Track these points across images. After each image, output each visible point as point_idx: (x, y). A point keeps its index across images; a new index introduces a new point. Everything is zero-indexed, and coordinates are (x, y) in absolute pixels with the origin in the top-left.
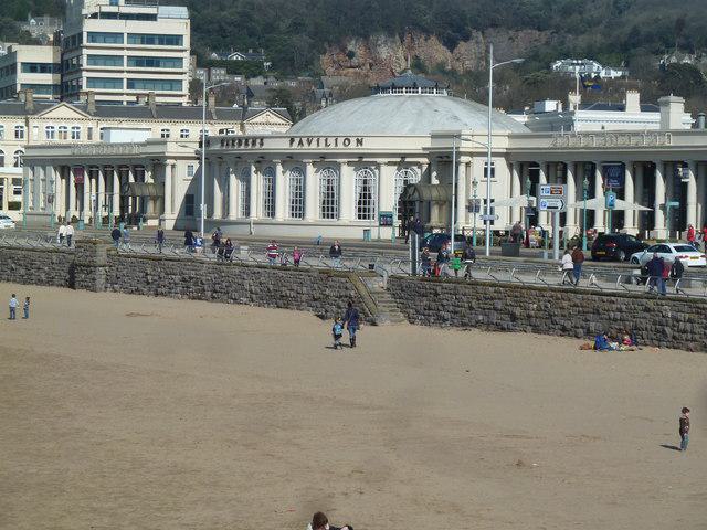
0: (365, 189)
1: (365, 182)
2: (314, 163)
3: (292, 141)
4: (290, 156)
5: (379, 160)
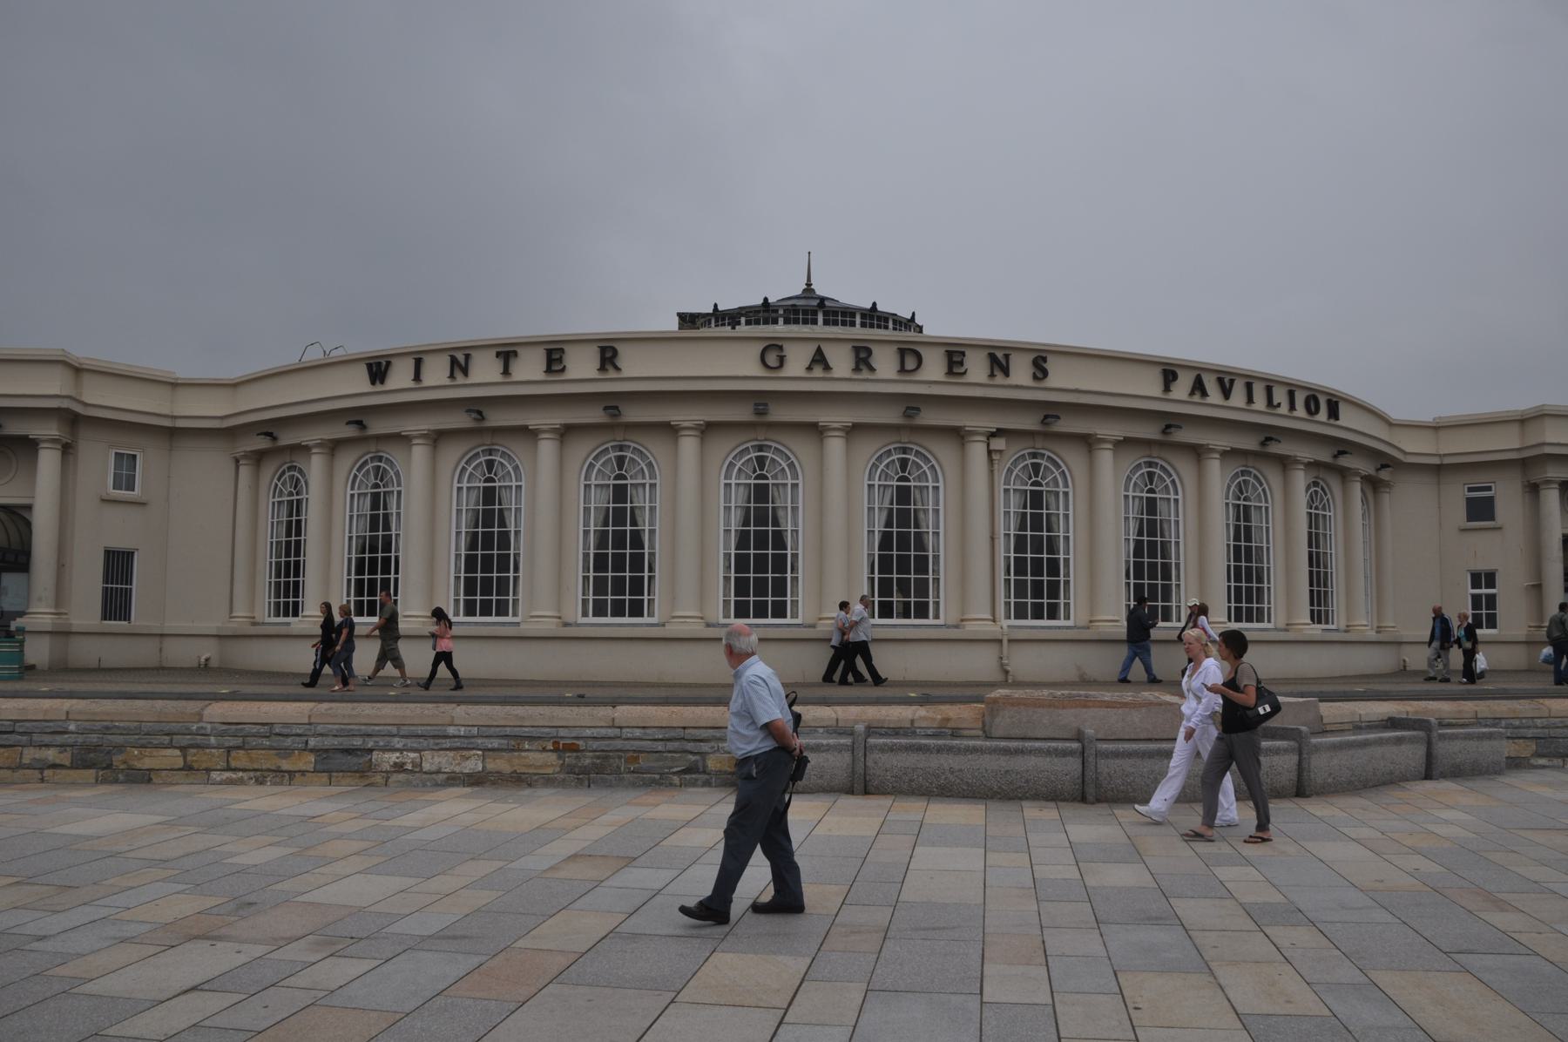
1: (375, 497)
4: (358, 417)
5: (534, 419)
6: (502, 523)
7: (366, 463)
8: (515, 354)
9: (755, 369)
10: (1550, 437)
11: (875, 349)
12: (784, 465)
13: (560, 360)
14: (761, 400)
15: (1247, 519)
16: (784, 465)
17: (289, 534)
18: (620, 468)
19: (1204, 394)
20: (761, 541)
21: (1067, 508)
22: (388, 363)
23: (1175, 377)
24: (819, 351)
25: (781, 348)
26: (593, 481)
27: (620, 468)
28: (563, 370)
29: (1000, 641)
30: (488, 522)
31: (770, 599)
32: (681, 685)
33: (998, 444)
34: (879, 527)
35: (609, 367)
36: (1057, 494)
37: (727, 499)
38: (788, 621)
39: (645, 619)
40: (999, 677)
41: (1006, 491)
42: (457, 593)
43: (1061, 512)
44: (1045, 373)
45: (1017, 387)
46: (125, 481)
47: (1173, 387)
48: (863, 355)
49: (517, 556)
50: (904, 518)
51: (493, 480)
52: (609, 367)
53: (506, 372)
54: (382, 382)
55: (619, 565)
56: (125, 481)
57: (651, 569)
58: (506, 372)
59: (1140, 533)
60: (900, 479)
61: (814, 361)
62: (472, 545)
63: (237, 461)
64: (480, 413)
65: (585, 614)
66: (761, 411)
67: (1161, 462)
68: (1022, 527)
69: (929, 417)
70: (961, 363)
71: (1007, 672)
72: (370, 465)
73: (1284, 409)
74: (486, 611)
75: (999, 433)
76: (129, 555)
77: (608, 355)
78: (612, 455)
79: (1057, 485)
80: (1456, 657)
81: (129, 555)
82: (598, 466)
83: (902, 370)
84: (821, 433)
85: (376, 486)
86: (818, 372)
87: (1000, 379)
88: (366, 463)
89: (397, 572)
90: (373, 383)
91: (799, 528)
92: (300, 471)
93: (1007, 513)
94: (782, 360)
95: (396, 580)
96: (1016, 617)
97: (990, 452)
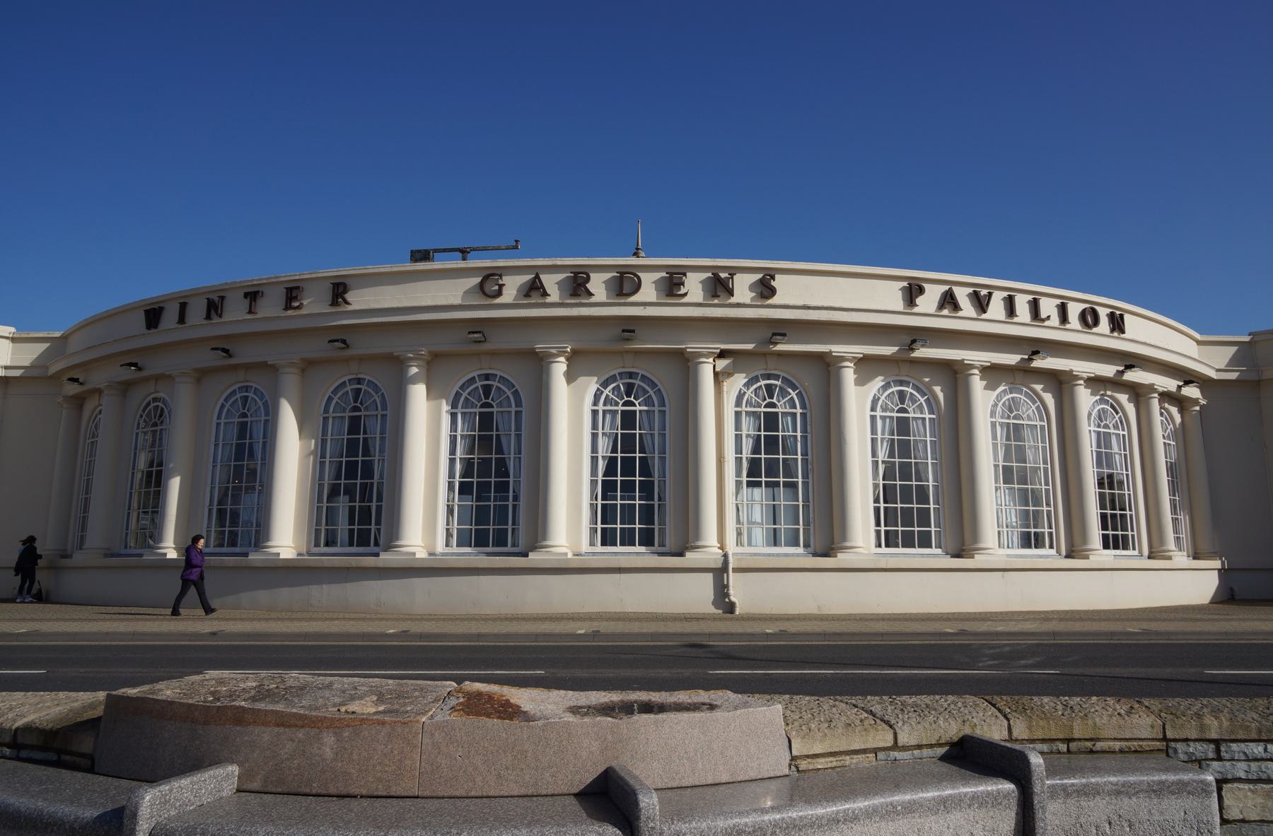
0: (352, 447)
2: (307, 366)
5: (837, 349)
10: (1191, 348)
12: (509, 393)
14: (479, 329)
15: (1019, 437)
16: (509, 393)
18: (487, 397)
19: (956, 307)
20: (905, 475)
23: (921, 291)
27: (487, 397)
31: (619, 526)
32: (486, 619)
34: (746, 453)
38: (509, 549)
41: (738, 414)
44: (773, 292)
45: (739, 305)
47: (919, 300)
49: (380, 485)
57: (380, 499)
60: (482, 406)
64: (344, 342)
65: (592, 544)
67: (912, 381)
72: (238, 396)
73: (1055, 320)
79: (510, 406)
82: (465, 394)
84: (542, 359)
88: (234, 392)
92: (164, 402)
93: (738, 438)
95: (878, 524)
96: (887, 545)
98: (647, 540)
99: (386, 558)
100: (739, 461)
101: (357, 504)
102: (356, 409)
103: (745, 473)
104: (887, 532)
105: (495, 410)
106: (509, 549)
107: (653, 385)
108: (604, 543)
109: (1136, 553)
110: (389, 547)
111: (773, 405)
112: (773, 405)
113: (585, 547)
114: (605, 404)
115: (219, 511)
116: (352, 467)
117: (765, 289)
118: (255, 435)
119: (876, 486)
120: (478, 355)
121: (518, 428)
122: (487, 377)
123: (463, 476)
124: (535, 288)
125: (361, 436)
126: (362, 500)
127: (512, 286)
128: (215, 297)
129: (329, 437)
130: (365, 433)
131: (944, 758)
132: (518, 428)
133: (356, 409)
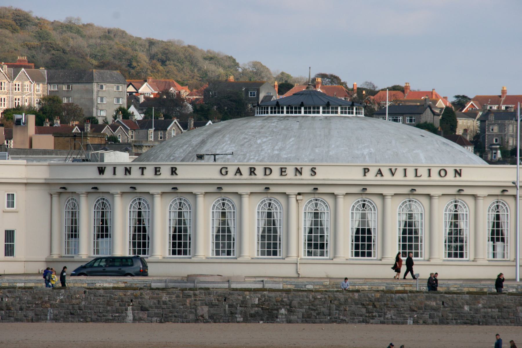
1: (103, 212)
3: (366, 171)
5: (336, 191)
6: (185, 224)
7: (69, 200)
8: (145, 168)
9: (218, 176)
11: (229, 167)
13: (159, 171)
17: (72, 224)
18: (316, 207)
20: (410, 233)
21: (508, 220)
22: (105, 168)
24: (239, 169)
25: (227, 168)
26: (307, 211)
27: (316, 207)
28: (160, 174)
29: (297, 264)
30: (140, 223)
33: (299, 197)
35: (252, 174)
36: (277, 212)
37: (213, 217)
39: (188, 256)
40: (297, 276)
42: (130, 247)
43: (506, 221)
46: (11, 204)
48: (252, 170)
50: (498, 225)
51: (270, 210)
52: (252, 174)
53: (142, 174)
54: (103, 174)
55: (363, 239)
56: (11, 204)
58: (142, 174)
59: (493, 227)
61: (237, 172)
62: (218, 231)
63: (51, 195)
66: (267, 188)
68: (175, 231)
69: (467, 191)
70: (285, 171)
71: (299, 274)
74: (180, 253)
75: (299, 194)
76: (13, 232)
77: (252, 170)
78: (137, 201)
80: (117, 318)
81: (13, 232)
82: (173, 205)
83: (265, 174)
85: (103, 209)
86: (238, 176)
87: (299, 176)
89: (190, 247)
90: (100, 174)
91: (468, 232)
92: (75, 201)
94: (227, 172)
97: (297, 200)
98: (229, 253)
99: (194, 259)
100: (305, 228)
101: (137, 248)
102: (180, 209)
103: (354, 233)
104: (231, 248)
105: (226, 211)
106: (278, 257)
107: (146, 202)
108: (217, 255)
109: (422, 259)
110: (194, 256)
111: (224, 209)
112: (224, 209)
113: (167, 255)
114: (262, 209)
115: (68, 242)
116: (269, 230)
117: (173, 171)
118: (145, 223)
119: (352, 236)
120: (267, 193)
121: (234, 217)
122: (223, 200)
123: (356, 234)
124: (239, 171)
125: (319, 219)
126: (452, 238)
127: (232, 170)
128: (128, 167)
129: (132, 218)
130: (415, 227)
131: (392, 268)
132: (234, 217)
133: (180, 209)
